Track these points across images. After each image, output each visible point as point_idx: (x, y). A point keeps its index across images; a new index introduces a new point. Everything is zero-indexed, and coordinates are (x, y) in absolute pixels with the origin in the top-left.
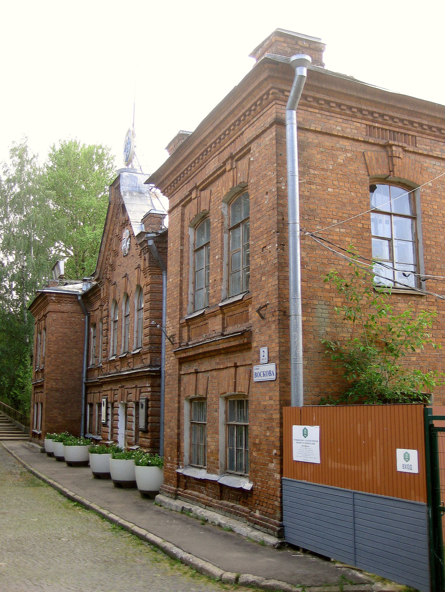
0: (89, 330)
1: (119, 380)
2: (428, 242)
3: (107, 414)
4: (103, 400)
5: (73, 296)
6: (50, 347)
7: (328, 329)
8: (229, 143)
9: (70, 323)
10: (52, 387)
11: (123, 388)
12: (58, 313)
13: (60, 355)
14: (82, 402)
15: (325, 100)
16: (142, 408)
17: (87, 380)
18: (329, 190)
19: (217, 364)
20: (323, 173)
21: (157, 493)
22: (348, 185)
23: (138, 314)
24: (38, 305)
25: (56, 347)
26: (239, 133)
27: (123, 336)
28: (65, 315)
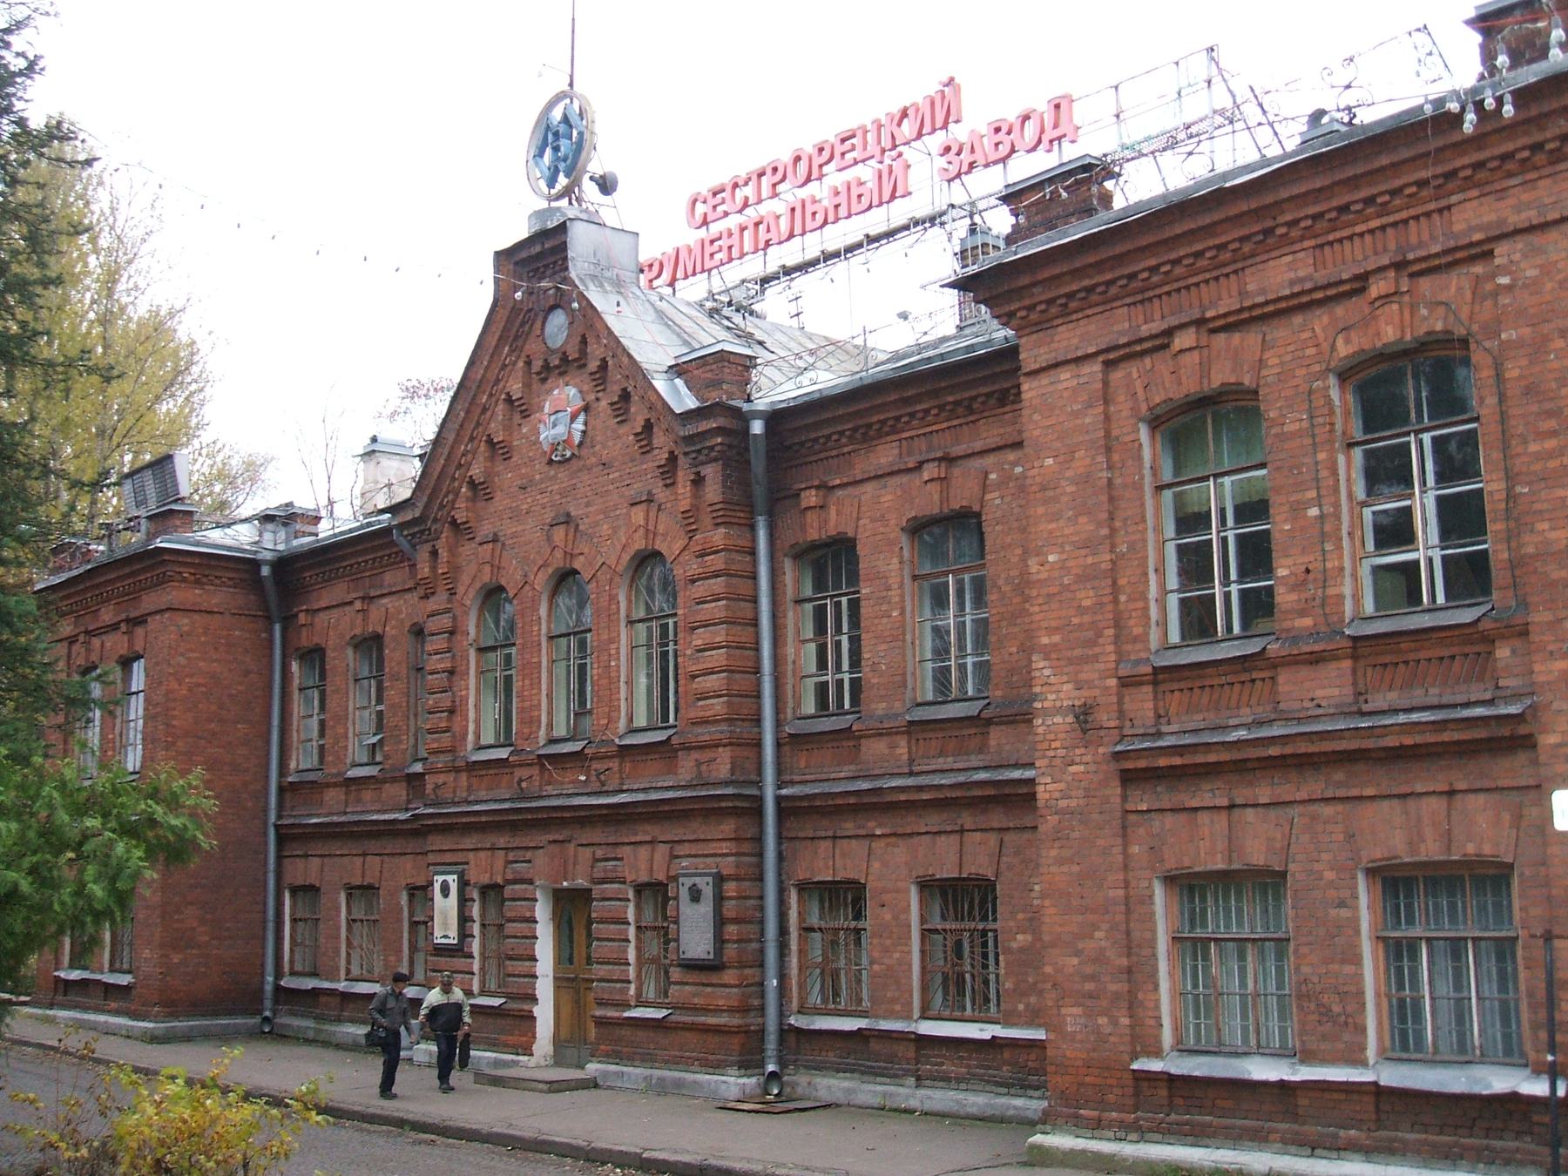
3: (464, 920)
4: (440, 878)
5: (241, 567)
6: (174, 717)
12: (196, 617)
17: (279, 817)
19: (1339, 785)
27: (544, 692)
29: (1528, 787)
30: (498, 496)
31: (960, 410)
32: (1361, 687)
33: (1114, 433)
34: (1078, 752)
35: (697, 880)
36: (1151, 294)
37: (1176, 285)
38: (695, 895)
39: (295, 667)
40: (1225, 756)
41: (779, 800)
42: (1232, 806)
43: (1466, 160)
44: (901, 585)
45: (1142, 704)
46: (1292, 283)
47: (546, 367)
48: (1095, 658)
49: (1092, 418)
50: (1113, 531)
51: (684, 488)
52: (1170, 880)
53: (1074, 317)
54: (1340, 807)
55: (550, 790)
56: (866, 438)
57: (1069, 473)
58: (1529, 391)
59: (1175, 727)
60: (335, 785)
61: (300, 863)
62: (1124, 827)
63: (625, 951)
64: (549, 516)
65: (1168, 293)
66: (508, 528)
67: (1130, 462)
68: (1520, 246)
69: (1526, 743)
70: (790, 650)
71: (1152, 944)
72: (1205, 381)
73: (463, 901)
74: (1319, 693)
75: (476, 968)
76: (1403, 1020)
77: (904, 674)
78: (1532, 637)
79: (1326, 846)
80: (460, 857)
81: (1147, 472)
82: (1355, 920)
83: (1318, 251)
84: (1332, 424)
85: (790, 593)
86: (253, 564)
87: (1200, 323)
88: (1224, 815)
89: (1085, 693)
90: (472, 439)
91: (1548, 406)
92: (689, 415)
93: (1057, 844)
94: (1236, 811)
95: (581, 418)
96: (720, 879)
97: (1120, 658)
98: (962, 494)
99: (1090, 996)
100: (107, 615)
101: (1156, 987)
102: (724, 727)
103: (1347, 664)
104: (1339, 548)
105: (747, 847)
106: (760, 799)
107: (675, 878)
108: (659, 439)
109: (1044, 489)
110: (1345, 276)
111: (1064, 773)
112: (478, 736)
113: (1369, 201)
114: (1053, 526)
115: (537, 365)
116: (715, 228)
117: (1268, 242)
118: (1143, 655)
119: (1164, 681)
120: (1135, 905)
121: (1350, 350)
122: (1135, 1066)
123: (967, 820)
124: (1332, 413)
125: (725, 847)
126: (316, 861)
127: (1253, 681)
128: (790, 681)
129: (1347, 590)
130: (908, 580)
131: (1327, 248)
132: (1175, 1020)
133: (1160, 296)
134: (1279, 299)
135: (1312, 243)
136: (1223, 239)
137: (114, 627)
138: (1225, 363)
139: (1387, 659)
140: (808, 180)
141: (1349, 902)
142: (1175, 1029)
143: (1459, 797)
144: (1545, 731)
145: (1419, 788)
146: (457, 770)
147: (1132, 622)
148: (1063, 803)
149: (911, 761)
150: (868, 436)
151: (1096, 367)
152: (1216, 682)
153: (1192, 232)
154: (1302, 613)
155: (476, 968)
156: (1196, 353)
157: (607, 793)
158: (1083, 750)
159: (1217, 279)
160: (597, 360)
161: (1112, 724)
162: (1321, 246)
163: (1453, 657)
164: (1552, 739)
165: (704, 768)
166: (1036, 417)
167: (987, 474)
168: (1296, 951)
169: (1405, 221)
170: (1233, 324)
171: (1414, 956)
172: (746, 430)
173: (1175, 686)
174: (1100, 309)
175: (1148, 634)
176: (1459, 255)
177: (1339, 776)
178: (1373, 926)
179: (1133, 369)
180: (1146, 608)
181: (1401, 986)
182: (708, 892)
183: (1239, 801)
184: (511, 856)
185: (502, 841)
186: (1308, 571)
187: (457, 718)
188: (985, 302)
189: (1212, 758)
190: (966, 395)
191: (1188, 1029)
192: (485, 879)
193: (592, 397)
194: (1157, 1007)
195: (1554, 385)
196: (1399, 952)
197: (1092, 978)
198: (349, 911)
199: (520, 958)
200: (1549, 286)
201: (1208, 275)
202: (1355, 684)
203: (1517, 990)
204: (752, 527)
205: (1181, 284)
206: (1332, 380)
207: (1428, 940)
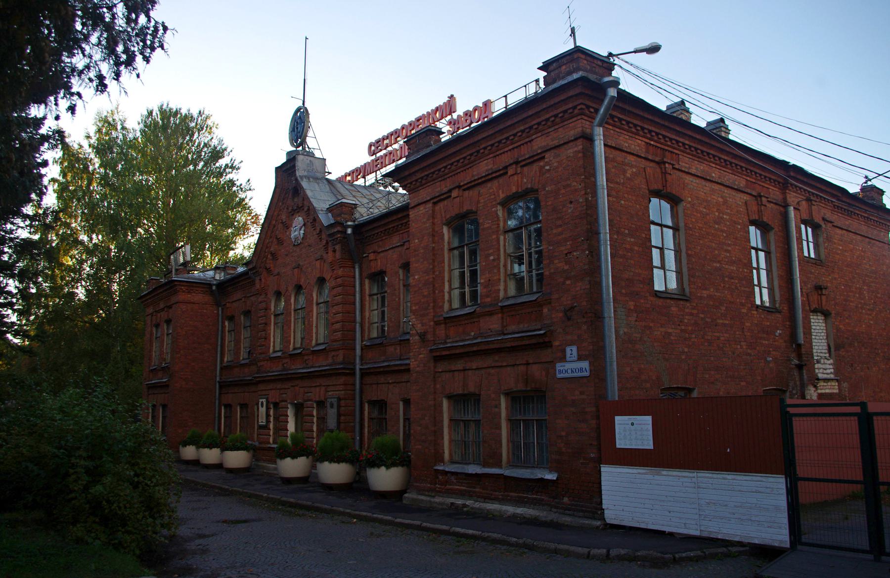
0: (223, 323)
1: (287, 378)
2: (690, 252)
3: (268, 415)
5: (205, 285)
7: (626, 330)
8: (510, 147)
11: (297, 388)
15: (619, 118)
18: (623, 202)
20: (617, 186)
21: (404, 491)
22: (634, 198)
26: (527, 140)
38: (332, 406)
39: (227, 323)
40: (462, 351)
41: (361, 369)
42: (464, 370)
43: (534, 122)
45: (441, 331)
47: (293, 210)
50: (434, 267)
51: (330, 253)
55: (293, 367)
70: (367, 314)
73: (268, 409)
75: (271, 433)
80: (267, 392)
81: (446, 244)
82: (500, 413)
85: (367, 292)
86: (210, 285)
92: (331, 226)
96: (339, 399)
100: (162, 306)
101: (443, 438)
104: (499, 271)
106: (354, 369)
107: (326, 399)
108: (324, 236)
109: (415, 251)
113: (507, 138)
116: (378, 155)
120: (438, 408)
122: (436, 468)
125: (341, 387)
128: (367, 325)
129: (502, 287)
130: (402, 287)
132: (450, 450)
137: (163, 309)
141: (498, 406)
151: (430, 205)
153: (454, 153)
154: (487, 296)
157: (308, 368)
160: (306, 209)
170: (470, 186)
172: (345, 232)
176: (535, 158)
178: (507, 415)
179: (441, 205)
184: (282, 392)
185: (279, 386)
189: (457, 351)
192: (273, 400)
202: (503, 322)
204: (354, 268)
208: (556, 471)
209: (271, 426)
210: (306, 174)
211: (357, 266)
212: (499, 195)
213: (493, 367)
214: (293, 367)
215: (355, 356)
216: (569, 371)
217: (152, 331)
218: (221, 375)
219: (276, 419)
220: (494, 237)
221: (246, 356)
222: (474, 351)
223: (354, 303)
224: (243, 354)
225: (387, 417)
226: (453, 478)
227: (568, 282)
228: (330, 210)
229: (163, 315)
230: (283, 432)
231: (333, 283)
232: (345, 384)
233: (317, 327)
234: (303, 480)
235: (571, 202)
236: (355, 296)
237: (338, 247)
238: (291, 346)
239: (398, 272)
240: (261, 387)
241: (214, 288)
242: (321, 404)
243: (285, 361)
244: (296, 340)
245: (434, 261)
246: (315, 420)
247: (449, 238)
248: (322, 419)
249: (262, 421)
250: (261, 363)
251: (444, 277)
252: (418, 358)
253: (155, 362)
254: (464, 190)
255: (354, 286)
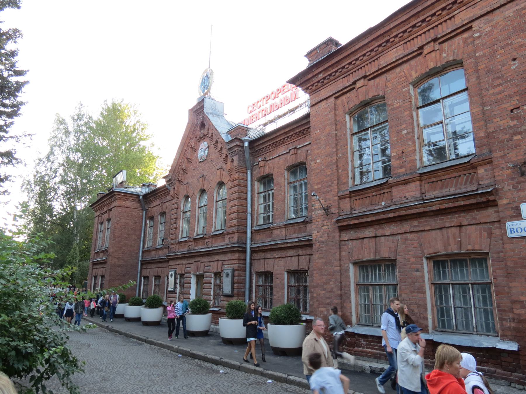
0: (146, 221)
3: (175, 283)
4: (171, 272)
5: (136, 196)
9: (131, 216)
10: (115, 263)
11: (199, 263)
13: (123, 240)
14: (137, 275)
16: (172, 277)
23: (199, 210)
24: (103, 202)
25: (120, 233)
28: (128, 210)
29: (494, 222)
30: (189, 173)
31: (301, 134)
32: (423, 191)
33: (338, 119)
34: (325, 222)
35: (228, 271)
36: (349, 73)
37: (357, 68)
38: (227, 276)
39: (148, 222)
41: (251, 248)
42: (376, 237)
44: (284, 186)
45: (346, 205)
46: (396, 57)
47: (200, 138)
48: (331, 191)
49: (331, 116)
50: (337, 150)
52: (355, 264)
53: (326, 86)
54: (416, 234)
55: (196, 248)
56: (276, 146)
57: (324, 134)
58: (489, 71)
59: (357, 212)
60: (154, 250)
61: (145, 270)
62: (340, 246)
63: (210, 292)
64: (199, 176)
65: (355, 71)
66: (190, 181)
67: (343, 127)
68: (483, 21)
69: (493, 204)
71: (349, 286)
72: (367, 96)
73: (176, 278)
74: (407, 195)
76: (443, 316)
77: (285, 211)
78: (495, 163)
79: (412, 248)
80: (175, 267)
81: (348, 130)
82: (423, 277)
83: (405, 45)
84: (411, 102)
85: (256, 191)
86: (138, 196)
87: (365, 77)
88: (373, 239)
89: (328, 202)
90: (183, 158)
91: (497, 75)
93: (318, 253)
94: (378, 238)
95: (207, 149)
96: (234, 271)
97: (339, 190)
98: (300, 159)
99: (328, 304)
100: (105, 209)
101: (350, 302)
102: (236, 227)
103: (418, 183)
105: (241, 262)
106: (246, 248)
107: (222, 271)
110: (415, 50)
111: (321, 231)
112: (182, 235)
113: (423, 21)
114: (319, 151)
115: (198, 137)
117: (388, 44)
118: (347, 188)
119: (353, 196)
120: (343, 273)
121: (417, 74)
123: (300, 252)
124: (411, 98)
125: (236, 261)
126: (148, 270)
127: (384, 193)
128: (256, 215)
129: (417, 157)
130: (286, 184)
131: (408, 43)
132: (357, 313)
133: (352, 73)
134: (392, 63)
135: (403, 42)
136: (372, 48)
137: (106, 212)
138: (374, 88)
139: (434, 179)
140: (275, 98)
141: (420, 270)
142: (357, 317)
143: (464, 228)
144: (501, 198)
145: (447, 225)
146: (176, 244)
147: (343, 178)
148: (321, 239)
149: (286, 236)
150: (276, 145)
152: (370, 195)
154: (401, 167)
155: (177, 297)
156: (364, 87)
158: (327, 221)
159: (371, 63)
161: (337, 211)
162: (406, 43)
163: (460, 176)
164: (505, 201)
165: (231, 239)
166: (314, 119)
167: (308, 151)
168: (400, 288)
169: (437, 26)
171: (446, 291)
173: (357, 198)
174: (334, 81)
175: (348, 181)
176: (458, 31)
177: (416, 223)
178: (430, 279)
179: (343, 98)
180: (348, 173)
181: (441, 303)
182: (230, 274)
183: (378, 235)
186: (403, 153)
187: (177, 230)
188: (299, 86)
189: (369, 219)
190: (301, 129)
191: (362, 317)
192: (180, 273)
193: (210, 144)
194: (351, 309)
195: (500, 67)
196: (440, 289)
197: (329, 298)
198: (155, 282)
199: (187, 294)
200: (496, 31)
201: (367, 62)
202: (421, 190)
203: (491, 305)
204: (247, 173)
205: (359, 67)
206: (411, 87)
207: (452, 284)
208: (518, 342)
209: (178, 291)
210: (211, 111)
211: (249, 172)
212: (411, 76)
213: (411, 232)
214: (196, 248)
215: (246, 238)
216: (519, 230)
217: (98, 226)
218: (142, 256)
219: (182, 286)
220: (408, 113)
221: (161, 242)
222: (390, 218)
223: (246, 199)
224: (159, 242)
225: (273, 285)
226: (362, 341)
227: (515, 138)
228: (229, 132)
229: (106, 216)
230: (187, 296)
231: (230, 184)
232: (239, 259)
233: (216, 218)
234: (205, 334)
235: (514, 60)
236: (247, 193)
237: (235, 158)
238: (195, 233)
239: (284, 173)
240: (171, 263)
241: (141, 197)
242: (218, 275)
243: (190, 244)
244: (199, 230)
245: (337, 145)
246: (212, 286)
247: (351, 125)
248: (219, 286)
249: (171, 287)
250: (173, 246)
251: (347, 157)
252: (321, 231)
253: (99, 247)
254: (369, 80)
255: (247, 187)
